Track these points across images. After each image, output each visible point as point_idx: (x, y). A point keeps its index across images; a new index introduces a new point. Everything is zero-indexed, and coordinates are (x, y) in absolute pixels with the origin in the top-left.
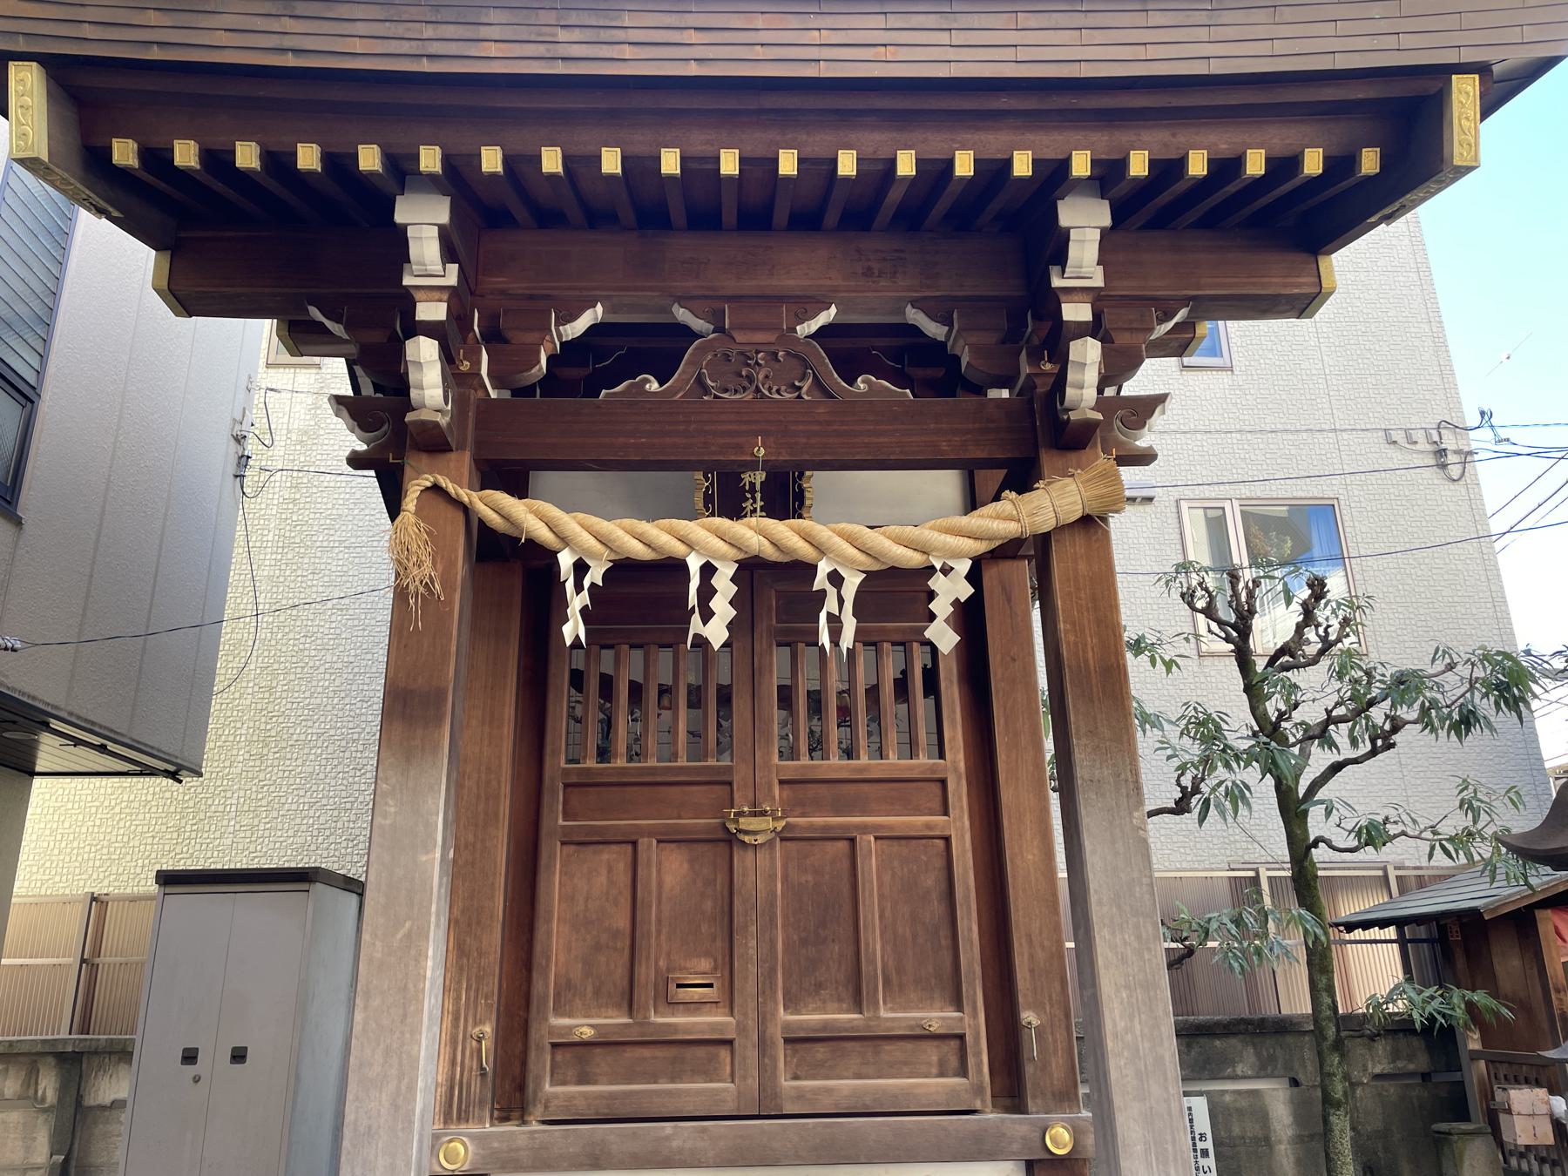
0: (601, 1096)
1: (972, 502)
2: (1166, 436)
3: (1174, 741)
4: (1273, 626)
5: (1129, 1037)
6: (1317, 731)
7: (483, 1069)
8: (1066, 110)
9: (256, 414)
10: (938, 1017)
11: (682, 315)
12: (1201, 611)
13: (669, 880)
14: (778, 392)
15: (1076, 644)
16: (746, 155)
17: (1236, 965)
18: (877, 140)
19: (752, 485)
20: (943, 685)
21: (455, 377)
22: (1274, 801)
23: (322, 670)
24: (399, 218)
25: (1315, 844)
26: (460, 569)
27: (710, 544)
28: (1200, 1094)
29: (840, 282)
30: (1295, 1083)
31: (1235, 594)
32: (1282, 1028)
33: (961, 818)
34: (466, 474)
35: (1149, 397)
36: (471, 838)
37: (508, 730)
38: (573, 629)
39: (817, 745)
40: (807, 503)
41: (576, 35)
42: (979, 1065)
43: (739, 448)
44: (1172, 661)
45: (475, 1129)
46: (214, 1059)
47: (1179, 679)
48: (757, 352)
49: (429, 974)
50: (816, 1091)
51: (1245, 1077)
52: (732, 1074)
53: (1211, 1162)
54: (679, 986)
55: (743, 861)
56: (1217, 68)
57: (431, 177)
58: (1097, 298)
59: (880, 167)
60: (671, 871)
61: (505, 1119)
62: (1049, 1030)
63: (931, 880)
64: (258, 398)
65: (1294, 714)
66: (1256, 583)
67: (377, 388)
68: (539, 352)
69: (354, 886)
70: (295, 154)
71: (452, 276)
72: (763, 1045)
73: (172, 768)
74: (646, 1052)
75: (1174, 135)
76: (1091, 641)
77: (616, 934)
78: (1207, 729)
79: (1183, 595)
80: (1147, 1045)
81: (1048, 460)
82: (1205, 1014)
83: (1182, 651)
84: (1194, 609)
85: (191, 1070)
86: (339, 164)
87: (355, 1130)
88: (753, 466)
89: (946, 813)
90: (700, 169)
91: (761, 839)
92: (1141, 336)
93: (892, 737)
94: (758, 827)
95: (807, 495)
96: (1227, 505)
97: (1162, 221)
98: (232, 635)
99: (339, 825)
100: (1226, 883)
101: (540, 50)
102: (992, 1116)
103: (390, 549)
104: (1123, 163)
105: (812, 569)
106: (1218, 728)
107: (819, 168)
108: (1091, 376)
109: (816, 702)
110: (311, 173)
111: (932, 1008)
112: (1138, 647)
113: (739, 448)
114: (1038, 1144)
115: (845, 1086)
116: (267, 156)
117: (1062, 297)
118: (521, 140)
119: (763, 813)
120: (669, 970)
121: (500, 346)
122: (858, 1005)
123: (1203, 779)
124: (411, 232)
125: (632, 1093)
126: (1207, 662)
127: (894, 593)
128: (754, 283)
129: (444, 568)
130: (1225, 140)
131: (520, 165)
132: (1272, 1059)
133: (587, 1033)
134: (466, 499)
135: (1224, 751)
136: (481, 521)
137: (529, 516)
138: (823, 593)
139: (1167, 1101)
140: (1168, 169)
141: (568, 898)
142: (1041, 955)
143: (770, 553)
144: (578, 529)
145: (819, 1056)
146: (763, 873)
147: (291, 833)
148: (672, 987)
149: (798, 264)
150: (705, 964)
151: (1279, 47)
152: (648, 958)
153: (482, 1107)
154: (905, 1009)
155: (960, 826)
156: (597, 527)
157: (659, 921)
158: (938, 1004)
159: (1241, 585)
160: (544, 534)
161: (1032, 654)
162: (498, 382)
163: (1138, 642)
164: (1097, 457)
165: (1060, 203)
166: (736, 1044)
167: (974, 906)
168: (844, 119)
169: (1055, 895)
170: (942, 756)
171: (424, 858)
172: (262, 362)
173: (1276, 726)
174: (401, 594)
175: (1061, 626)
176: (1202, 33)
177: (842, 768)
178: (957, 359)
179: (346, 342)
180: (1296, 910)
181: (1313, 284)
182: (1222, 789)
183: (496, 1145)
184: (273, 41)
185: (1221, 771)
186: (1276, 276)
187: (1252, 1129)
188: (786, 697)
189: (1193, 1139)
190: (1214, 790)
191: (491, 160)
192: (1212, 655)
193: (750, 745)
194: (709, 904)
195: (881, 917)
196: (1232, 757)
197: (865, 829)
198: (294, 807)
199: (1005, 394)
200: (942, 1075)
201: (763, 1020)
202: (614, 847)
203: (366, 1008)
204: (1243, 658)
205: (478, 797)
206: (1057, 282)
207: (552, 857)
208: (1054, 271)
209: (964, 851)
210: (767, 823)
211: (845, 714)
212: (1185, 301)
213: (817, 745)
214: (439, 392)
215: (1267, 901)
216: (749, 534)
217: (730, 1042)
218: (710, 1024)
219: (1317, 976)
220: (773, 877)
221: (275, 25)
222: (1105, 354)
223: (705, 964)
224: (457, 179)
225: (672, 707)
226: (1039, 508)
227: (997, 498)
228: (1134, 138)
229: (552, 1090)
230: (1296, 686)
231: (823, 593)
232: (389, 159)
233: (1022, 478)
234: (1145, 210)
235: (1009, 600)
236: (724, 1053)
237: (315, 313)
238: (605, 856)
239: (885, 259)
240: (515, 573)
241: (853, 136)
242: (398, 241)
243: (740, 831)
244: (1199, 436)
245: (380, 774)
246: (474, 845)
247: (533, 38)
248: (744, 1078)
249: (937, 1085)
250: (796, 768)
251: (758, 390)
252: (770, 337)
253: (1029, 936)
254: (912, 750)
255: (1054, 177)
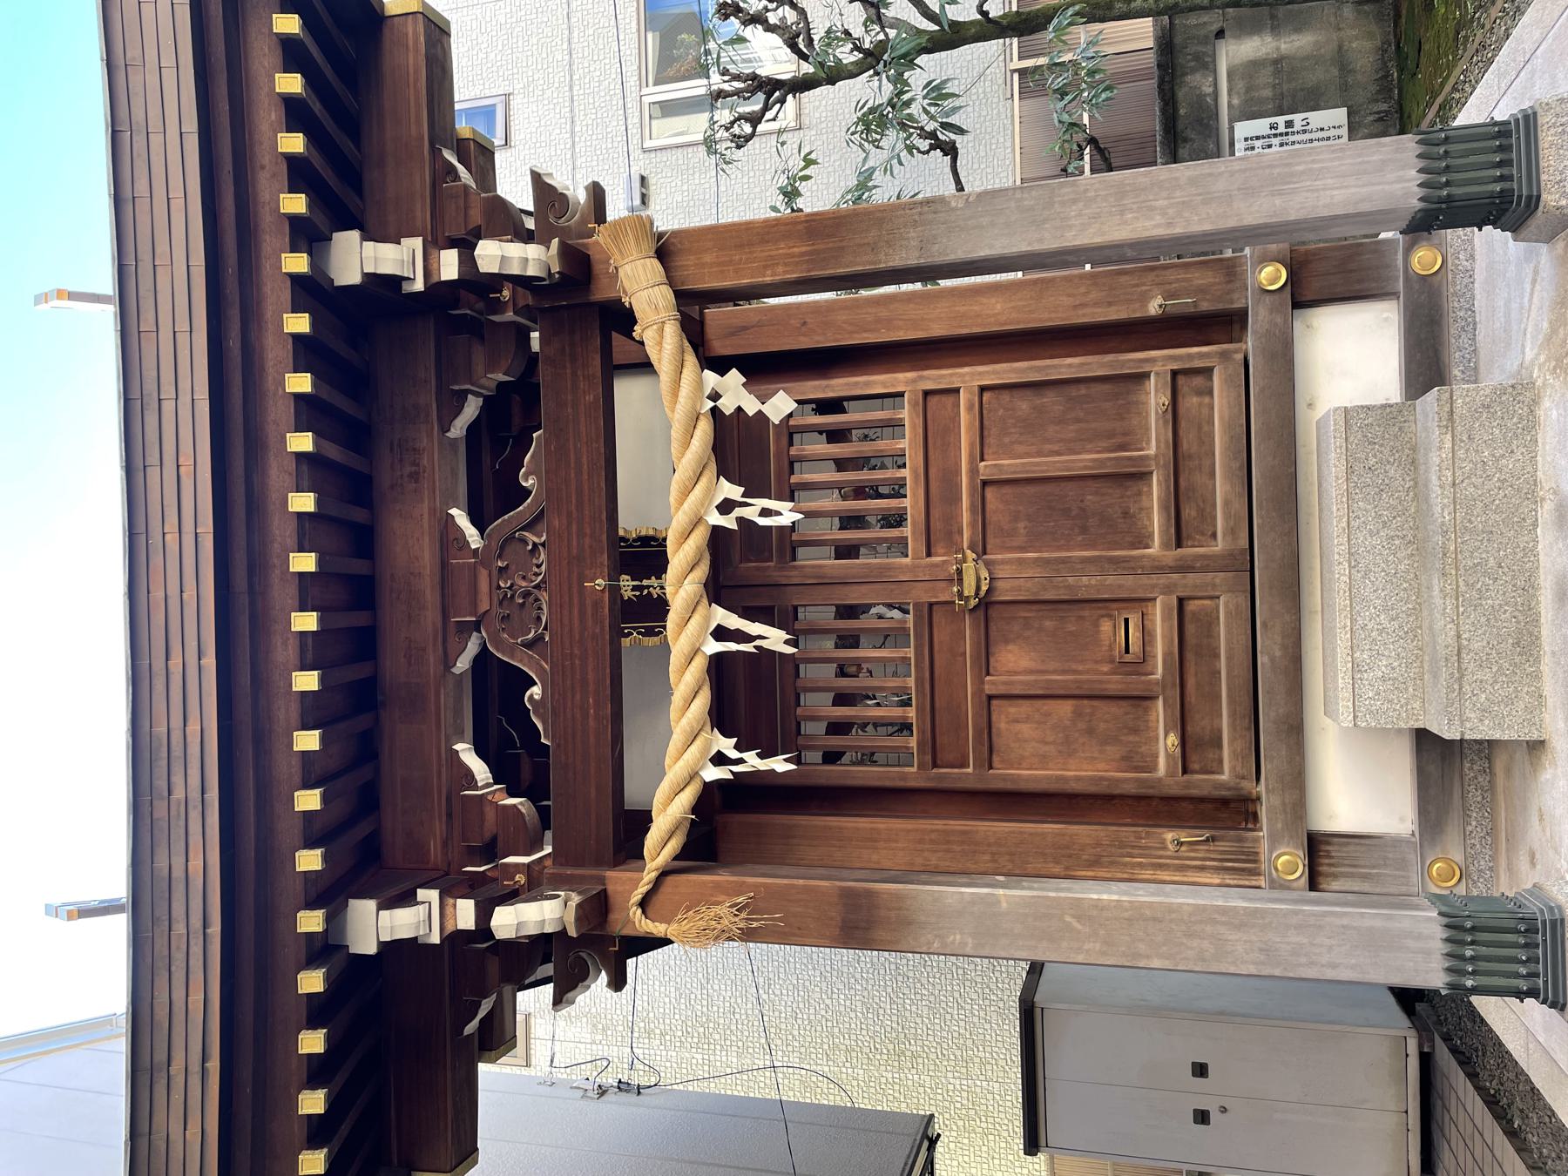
0: (1233, 726)
1: (644, 366)
2: (578, 163)
3: (885, 155)
4: (770, 56)
5: (1170, 211)
6: (872, 11)
7: (1207, 840)
8: (240, 283)
9: (577, 1076)
10: (1155, 397)
11: (463, 664)
12: (754, 128)
13: (1025, 662)
14: (539, 566)
15: (786, 265)
16: (297, 605)
17: (1104, 96)
18: (277, 473)
19: (634, 588)
20: (831, 395)
21: (533, 887)
22: (944, 54)
23: (828, 1002)
24: (372, 949)
25: (985, 14)
26: (723, 877)
27: (694, 629)
28: (1232, 129)
29: (426, 504)
30: (1220, 34)
31: (737, 93)
32: (1167, 46)
33: (963, 375)
34: (628, 874)
35: (535, 190)
36: (987, 857)
37: (882, 824)
38: (779, 765)
39: (895, 520)
40: (651, 533)
41: (178, 779)
42: (1201, 356)
43: (597, 605)
44: (805, 159)
45: (1264, 846)
46: (1204, 1094)
47: (821, 154)
48: (499, 587)
49: (1115, 897)
50: (1227, 516)
51: (1215, 84)
52: (1211, 598)
53: (1297, 118)
54: (1127, 651)
55: (1005, 592)
56: (191, 125)
57: (328, 919)
58: (434, 244)
59: (305, 468)
60: (1016, 662)
61: (1255, 817)
62: (1168, 287)
63: (1023, 405)
64: (561, 1075)
65: (855, 35)
66: (725, 72)
67: (546, 960)
68: (505, 806)
69: (1036, 969)
70: (309, 1116)
71: (430, 895)
72: (1183, 568)
73: (926, 1144)
74: (1191, 682)
75: (263, 167)
76: (782, 249)
77: (1078, 714)
78: (872, 123)
79: (739, 147)
80: (1178, 194)
81: (601, 293)
82: (1154, 124)
83: (796, 146)
84: (753, 135)
85: (1215, 1116)
86: (317, 1011)
87: (1263, 963)
88: (615, 590)
89: (957, 391)
90: (312, 652)
91: (984, 574)
92: (472, 197)
93: (884, 445)
94: (973, 576)
95: (643, 533)
96: (646, 100)
97: (353, 176)
98: (794, 1091)
99: (979, 979)
100: (1024, 102)
101: (195, 816)
102: (1250, 343)
103: (705, 946)
104: (293, 219)
105: (716, 531)
106: (872, 110)
107: (308, 530)
108: (515, 250)
109: (851, 521)
110: (328, 1039)
111: (1146, 403)
112: (790, 194)
113: (597, 605)
114: (1276, 297)
115: (1222, 488)
116: (312, 1083)
117: (435, 279)
118: (289, 831)
119: (960, 572)
120: (1112, 661)
121: (500, 844)
122: (1144, 476)
123: (922, 128)
124: (386, 938)
125: (1229, 696)
126: (806, 121)
127: (739, 449)
128: (428, 592)
129: (724, 891)
130: (267, 116)
131: (314, 831)
133: (1173, 739)
134: (654, 875)
135: (893, 107)
136: (676, 858)
137: (670, 812)
138: (740, 520)
139: (1232, 174)
140: (298, 173)
141: (1044, 761)
142: (1094, 295)
143: (702, 572)
144: (681, 763)
145: (1193, 513)
146: (1017, 571)
147: (987, 1026)
148: (1128, 658)
149: (409, 547)
150: (1106, 626)
151: (168, 61)
152: (1101, 682)
153: (1240, 840)
154: (1148, 429)
155: (969, 377)
156: (679, 745)
157: (1064, 672)
158: (1143, 398)
159: (726, 87)
160: (687, 797)
161: (799, 305)
162: (537, 845)
163: (785, 194)
164: (597, 242)
165: (337, 283)
166: (1181, 594)
167: (1048, 362)
168: (256, 506)
169: (1035, 282)
170: (901, 395)
171: (1004, 905)
172: (525, 1071)
173: (868, 53)
174: (748, 935)
175: (768, 279)
176: (156, 140)
177: (914, 495)
178: (501, 385)
179: (500, 997)
180: (1049, 34)
181: (415, 22)
182: (932, 110)
183: (1280, 825)
184: (195, 1081)
185: (914, 110)
186: (408, 58)
187: (1265, 76)
188: (846, 551)
189: (1275, 135)
190: (932, 118)
191: (310, 860)
192: (799, 116)
193: (893, 586)
194: (1048, 623)
195: (1058, 453)
196: (898, 101)
197: (973, 471)
198: (962, 1024)
199: (535, 335)
200: (1210, 393)
201: (1159, 568)
202: (994, 718)
203: (1148, 957)
204: (801, 85)
205: (948, 851)
206: (419, 286)
207: (1004, 778)
208: (407, 288)
209: (994, 372)
210: (969, 569)
211: (860, 492)
212: (435, 154)
213: (896, 520)
214: (546, 903)
215: (1042, 61)
216: (682, 593)
217: (1181, 601)
218: (1163, 620)
219: (1116, 12)
220: (1020, 561)
221: (178, 1081)
222: (492, 235)
223: (1106, 626)
224: (330, 893)
225: (858, 663)
226: (650, 302)
227: (642, 343)
228: (267, 208)
229: (1227, 773)
230: (829, 32)
231: (740, 520)
232: (311, 963)
233: (621, 318)
234: (343, 192)
235: (745, 328)
236: (1191, 606)
237: (471, 1028)
238: (1003, 726)
239: (401, 460)
240: (725, 824)
241: (274, 496)
242: (397, 951)
243: (977, 594)
244: (577, 129)
245: (924, 949)
246: (993, 854)
247: (182, 823)
248: (1214, 586)
249: (1221, 397)
250: (915, 540)
251: (537, 587)
252: (483, 574)
253: (1075, 307)
254: (895, 425)
255: (311, 291)
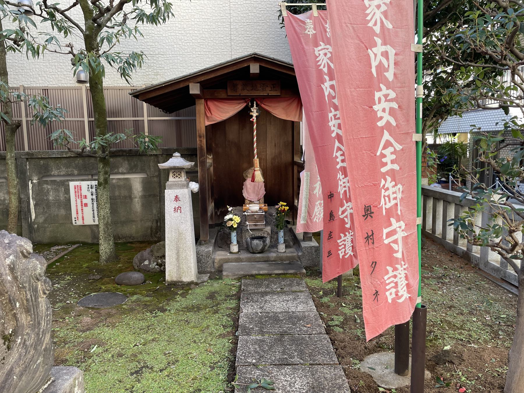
132: (136, 166)
187: (124, 193)
